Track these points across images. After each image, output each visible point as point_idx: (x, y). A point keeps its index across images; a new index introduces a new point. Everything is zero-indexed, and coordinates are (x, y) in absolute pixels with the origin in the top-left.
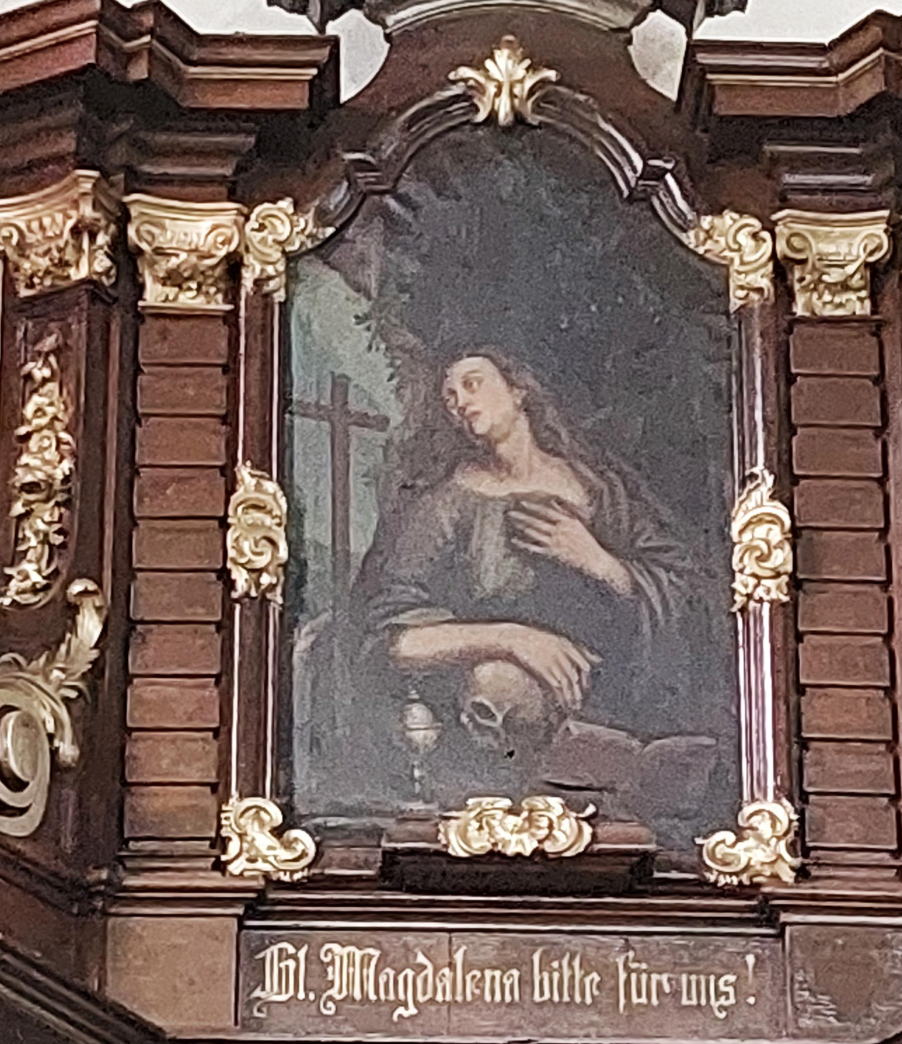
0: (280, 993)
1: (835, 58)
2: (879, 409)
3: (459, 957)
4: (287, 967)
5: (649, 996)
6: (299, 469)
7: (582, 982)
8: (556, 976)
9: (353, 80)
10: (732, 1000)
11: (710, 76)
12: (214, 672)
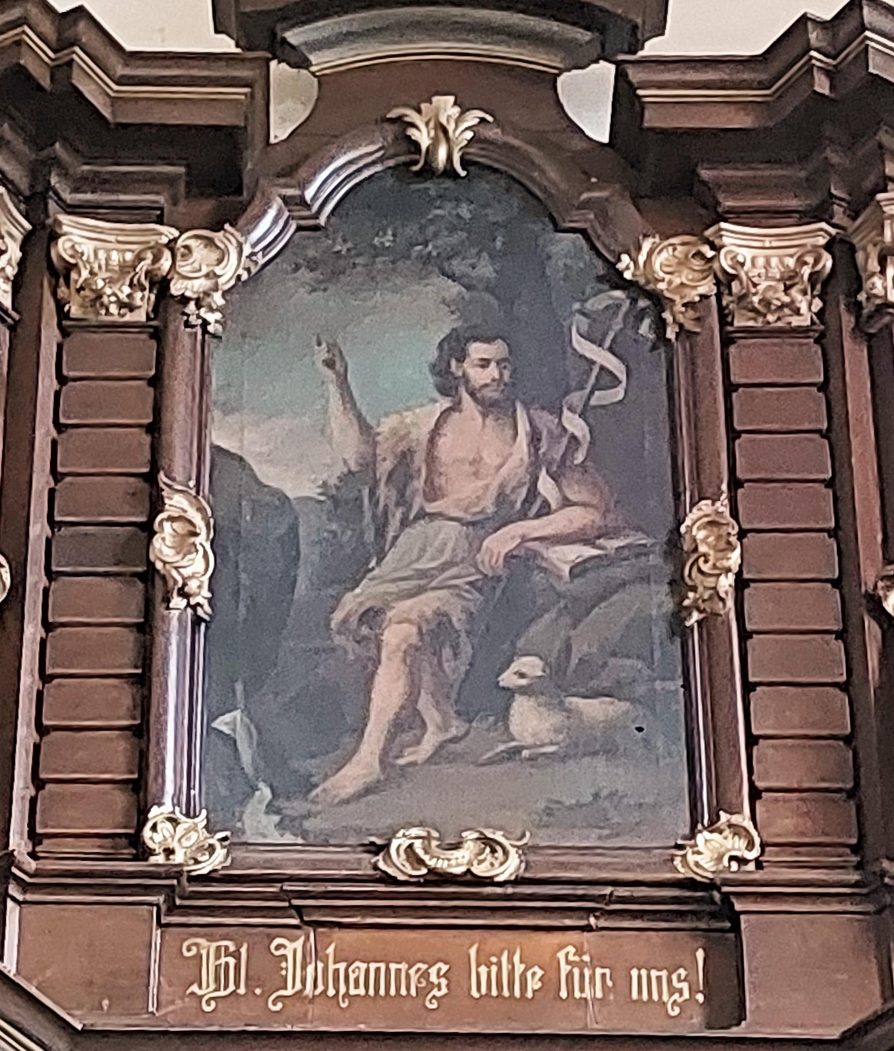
0: (217, 989)
1: (776, 65)
2: (869, 395)
3: (330, 951)
4: (227, 964)
5: (367, 987)
6: (866, 409)
7: (523, 976)
8: (494, 969)
9: (283, 120)
10: (444, 990)
11: (640, 92)
12: (835, 628)
